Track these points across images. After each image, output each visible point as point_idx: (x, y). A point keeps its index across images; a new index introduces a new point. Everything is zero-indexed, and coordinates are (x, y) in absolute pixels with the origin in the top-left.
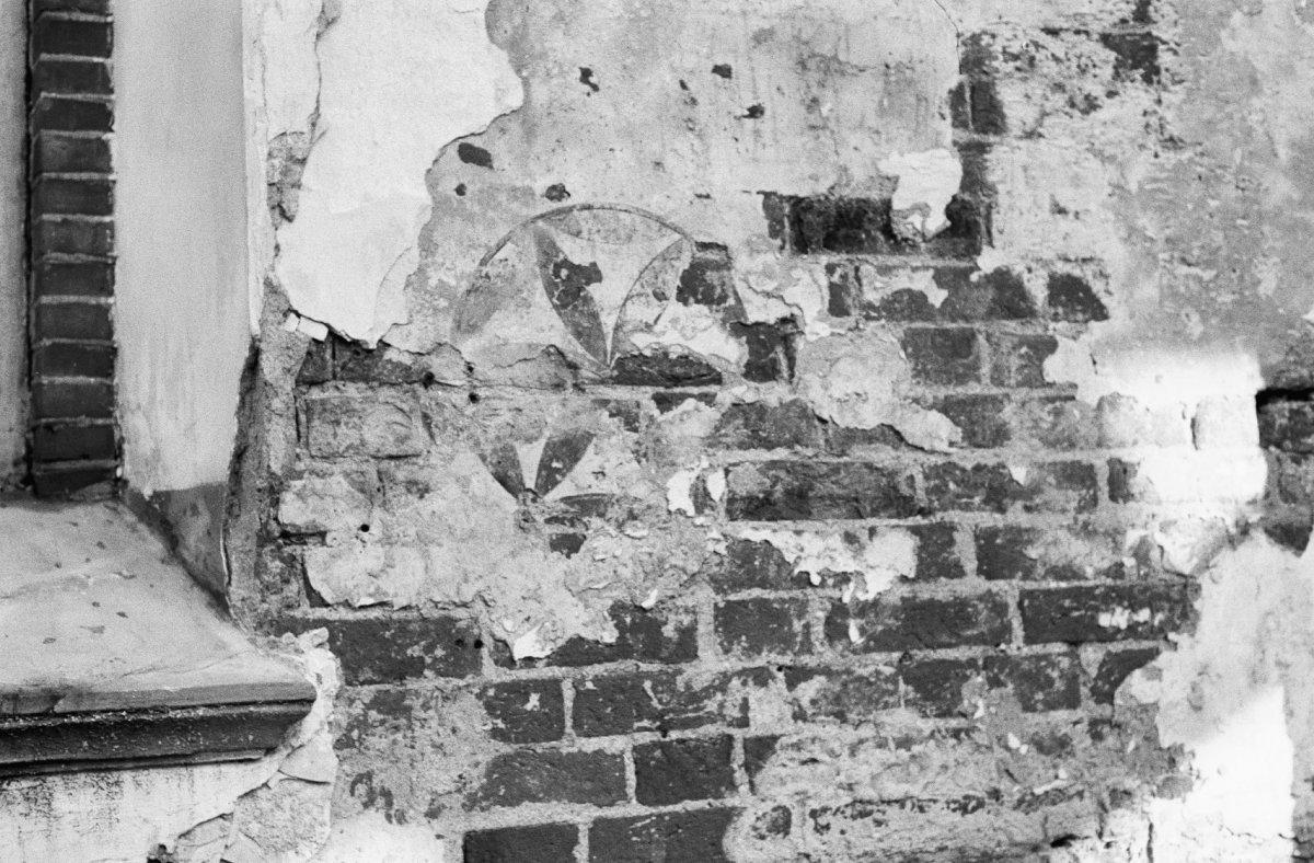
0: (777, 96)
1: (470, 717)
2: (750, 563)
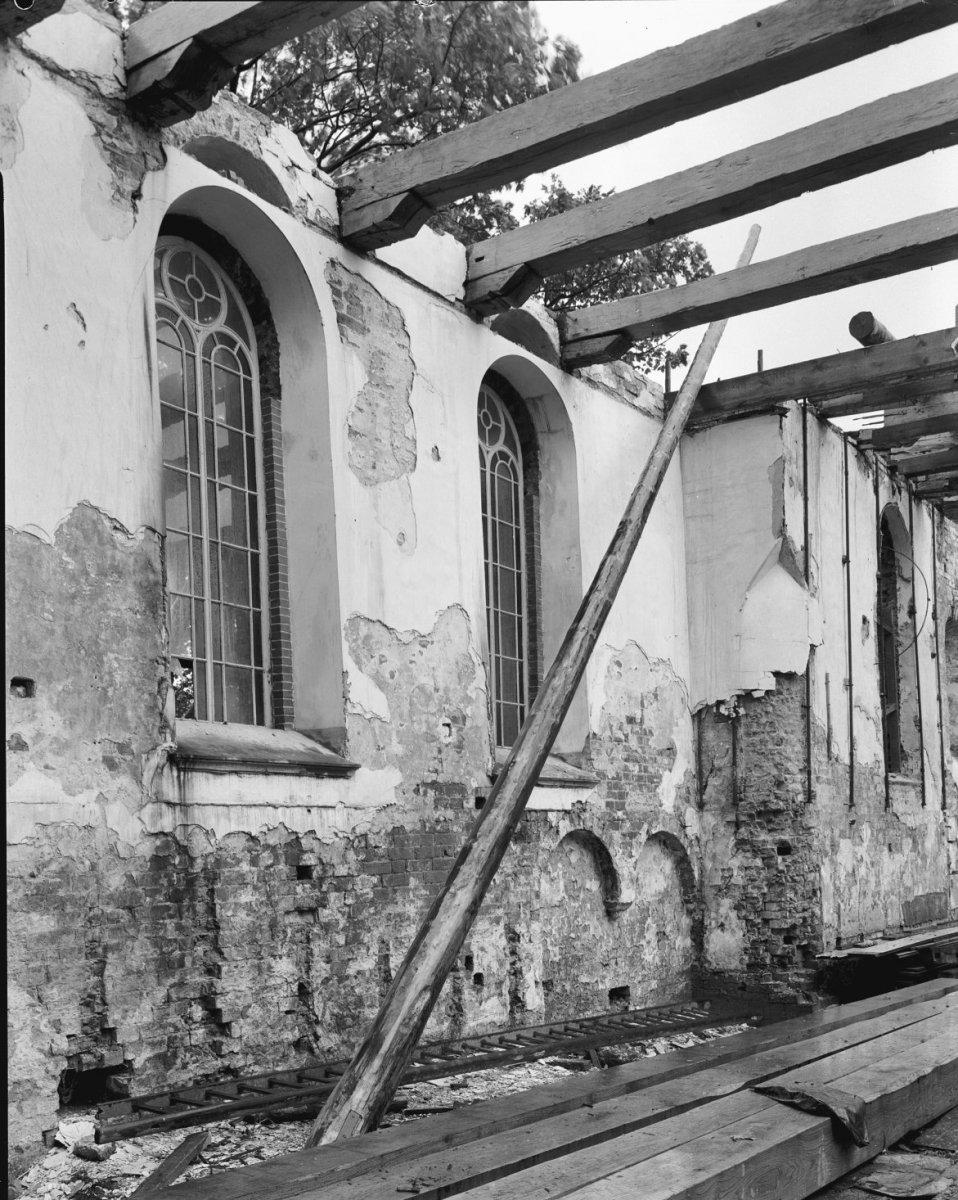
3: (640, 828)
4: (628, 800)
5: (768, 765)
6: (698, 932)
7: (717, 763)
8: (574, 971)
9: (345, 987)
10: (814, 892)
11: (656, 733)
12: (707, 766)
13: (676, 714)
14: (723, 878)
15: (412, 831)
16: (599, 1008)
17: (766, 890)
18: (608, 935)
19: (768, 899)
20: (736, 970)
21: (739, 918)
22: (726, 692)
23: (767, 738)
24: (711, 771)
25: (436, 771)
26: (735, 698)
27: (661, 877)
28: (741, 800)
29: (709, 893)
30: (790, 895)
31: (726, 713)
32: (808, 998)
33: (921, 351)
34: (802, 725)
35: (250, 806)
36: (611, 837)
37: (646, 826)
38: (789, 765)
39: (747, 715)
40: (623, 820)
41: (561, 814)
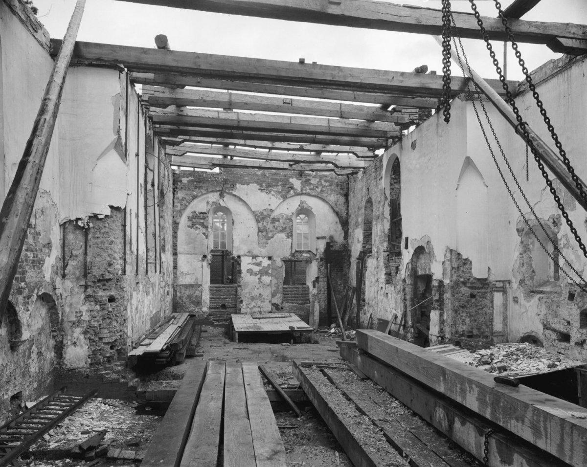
3: (33, 292)
4: (28, 275)
5: (105, 255)
6: (59, 349)
7: (74, 252)
10: (125, 321)
11: (42, 234)
12: (68, 254)
13: (52, 223)
14: (76, 317)
17: (101, 322)
19: (102, 326)
20: (83, 368)
21: (85, 338)
22: (82, 213)
23: (105, 241)
24: (71, 257)
26: (88, 218)
27: (40, 320)
28: (89, 273)
29: (67, 326)
30: (115, 324)
31: (82, 225)
32: (124, 377)
33: (197, 60)
34: (122, 234)
36: (17, 299)
37: (36, 291)
38: (115, 255)
39: (93, 227)
40: (24, 288)
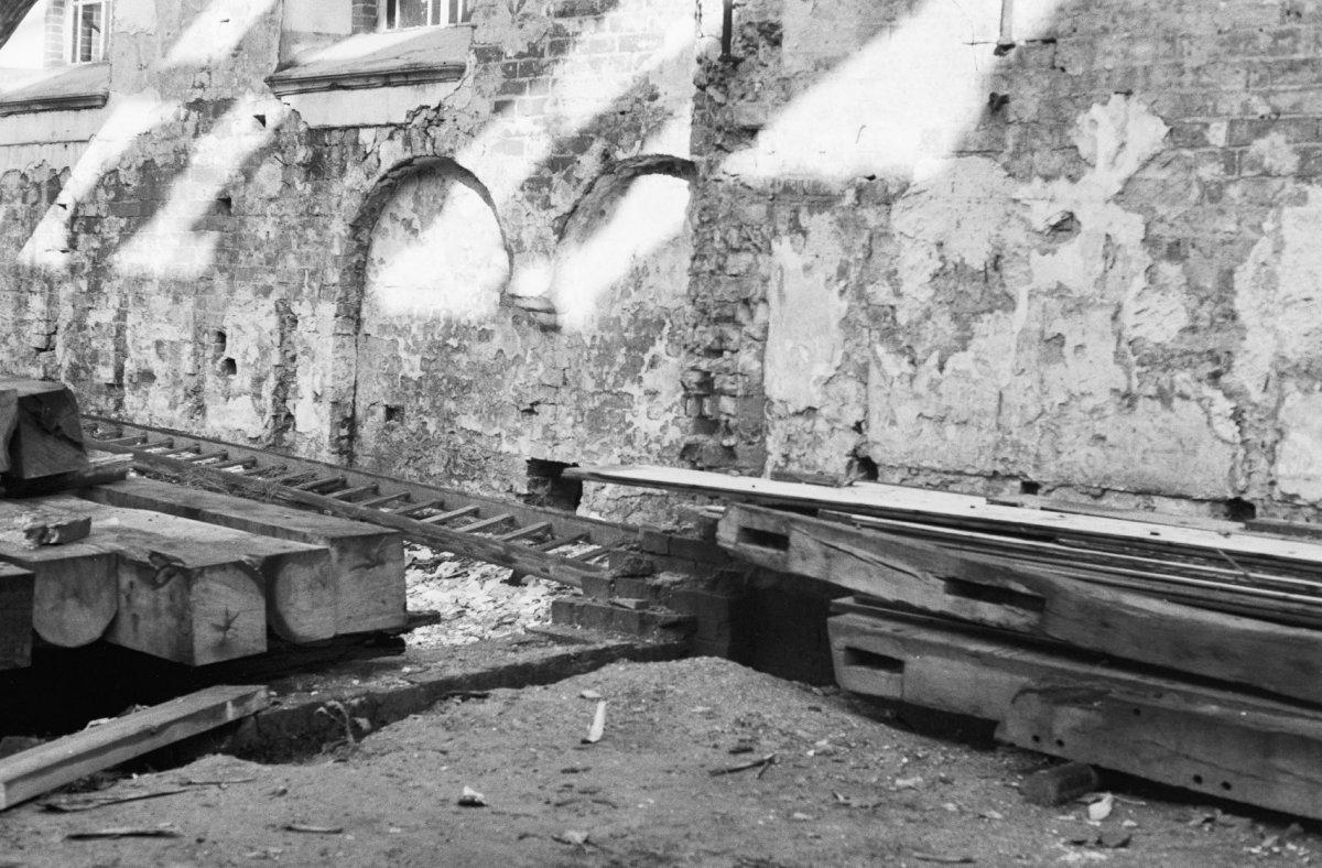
0: (279, 810)
1: (499, 73)
2: (558, 30)
8: (451, 405)
9: (84, 337)
15: (165, 165)
16: (496, 484)
18: (537, 357)
25: (202, 86)
35: (22, 145)
41: (387, 131)
